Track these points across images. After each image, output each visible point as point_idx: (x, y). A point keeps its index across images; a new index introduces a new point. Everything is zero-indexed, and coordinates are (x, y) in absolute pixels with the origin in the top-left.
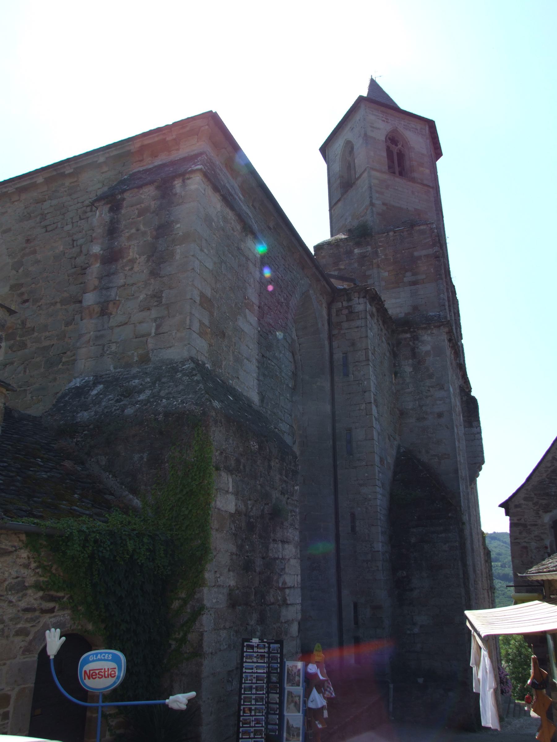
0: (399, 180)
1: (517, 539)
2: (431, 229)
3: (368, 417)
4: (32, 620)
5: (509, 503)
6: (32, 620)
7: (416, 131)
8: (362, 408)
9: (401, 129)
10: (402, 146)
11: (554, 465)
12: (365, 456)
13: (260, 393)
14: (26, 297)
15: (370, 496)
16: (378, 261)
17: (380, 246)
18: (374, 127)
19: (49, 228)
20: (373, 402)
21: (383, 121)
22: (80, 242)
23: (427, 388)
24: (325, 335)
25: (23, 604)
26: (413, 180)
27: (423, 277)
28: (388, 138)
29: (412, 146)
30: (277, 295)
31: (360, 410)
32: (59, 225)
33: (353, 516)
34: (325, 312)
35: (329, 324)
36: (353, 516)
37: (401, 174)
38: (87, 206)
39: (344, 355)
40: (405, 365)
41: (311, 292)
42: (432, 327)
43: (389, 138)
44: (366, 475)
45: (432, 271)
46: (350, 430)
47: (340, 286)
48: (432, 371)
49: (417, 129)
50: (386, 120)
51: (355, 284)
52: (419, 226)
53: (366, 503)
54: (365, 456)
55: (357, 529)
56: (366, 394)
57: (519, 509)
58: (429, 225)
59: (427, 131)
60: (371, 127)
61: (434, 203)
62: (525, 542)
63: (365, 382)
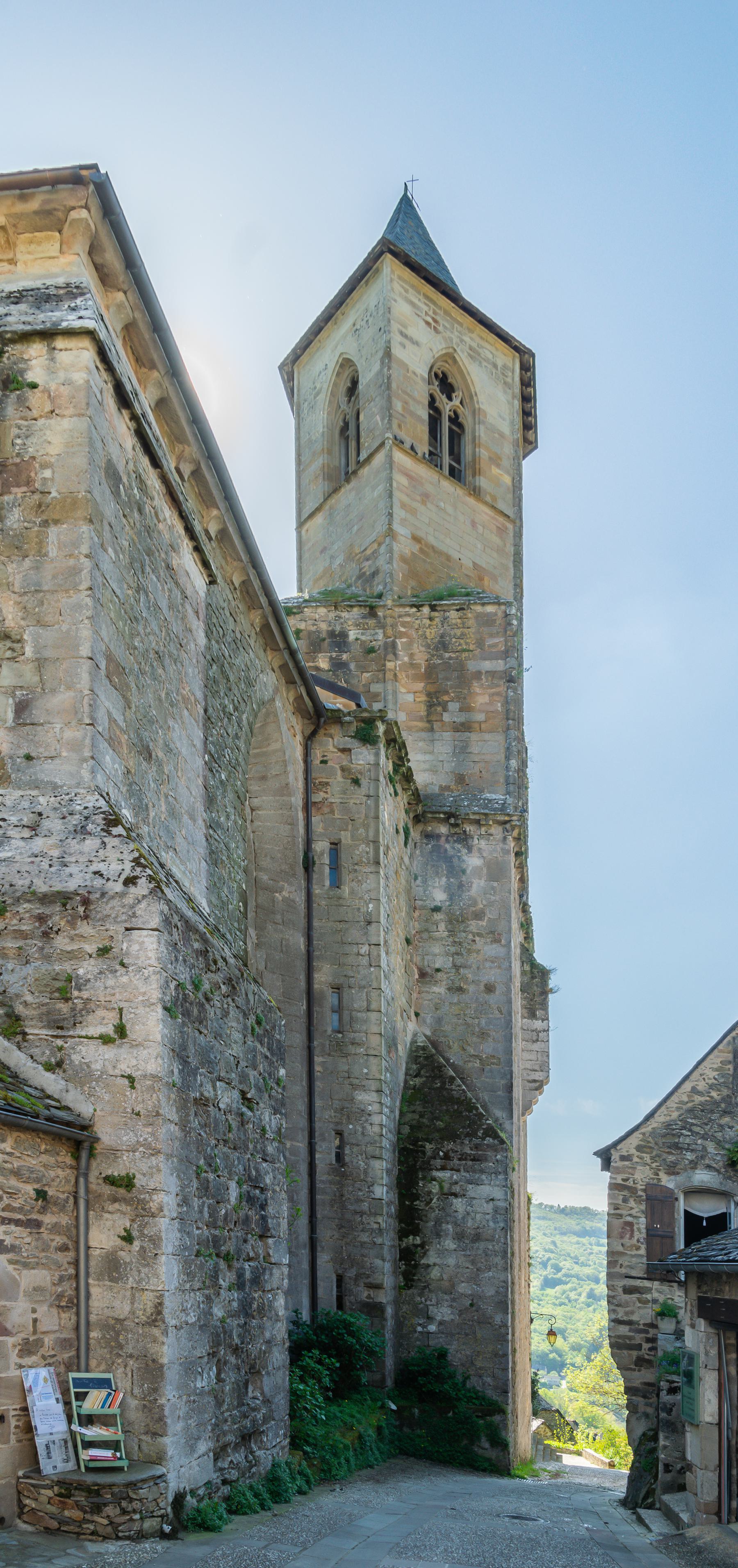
0: (448, 485)
1: (618, 1209)
2: (506, 615)
3: (372, 969)
5: (613, 1151)
7: (494, 371)
8: (362, 951)
9: (463, 357)
11: (693, 1101)
12: (364, 1039)
15: (370, 1108)
16: (396, 667)
17: (402, 635)
18: (406, 336)
20: (382, 944)
21: (428, 323)
23: (470, 937)
24: (298, 800)
26: (476, 492)
27: (481, 717)
28: (433, 374)
29: (481, 406)
30: (222, 694)
31: (358, 954)
34: (298, 753)
35: (306, 779)
37: (455, 474)
39: (333, 846)
40: (434, 887)
41: (278, 704)
42: (491, 823)
43: (436, 375)
44: (365, 1071)
45: (500, 709)
46: (338, 989)
48: (482, 906)
50: (433, 324)
51: (358, 705)
52: (483, 604)
53: (363, 1118)
54: (364, 1039)
55: (347, 1159)
56: (372, 928)
57: (627, 1163)
58: (503, 607)
60: (401, 333)
61: (512, 558)
62: (630, 1215)
63: (371, 906)
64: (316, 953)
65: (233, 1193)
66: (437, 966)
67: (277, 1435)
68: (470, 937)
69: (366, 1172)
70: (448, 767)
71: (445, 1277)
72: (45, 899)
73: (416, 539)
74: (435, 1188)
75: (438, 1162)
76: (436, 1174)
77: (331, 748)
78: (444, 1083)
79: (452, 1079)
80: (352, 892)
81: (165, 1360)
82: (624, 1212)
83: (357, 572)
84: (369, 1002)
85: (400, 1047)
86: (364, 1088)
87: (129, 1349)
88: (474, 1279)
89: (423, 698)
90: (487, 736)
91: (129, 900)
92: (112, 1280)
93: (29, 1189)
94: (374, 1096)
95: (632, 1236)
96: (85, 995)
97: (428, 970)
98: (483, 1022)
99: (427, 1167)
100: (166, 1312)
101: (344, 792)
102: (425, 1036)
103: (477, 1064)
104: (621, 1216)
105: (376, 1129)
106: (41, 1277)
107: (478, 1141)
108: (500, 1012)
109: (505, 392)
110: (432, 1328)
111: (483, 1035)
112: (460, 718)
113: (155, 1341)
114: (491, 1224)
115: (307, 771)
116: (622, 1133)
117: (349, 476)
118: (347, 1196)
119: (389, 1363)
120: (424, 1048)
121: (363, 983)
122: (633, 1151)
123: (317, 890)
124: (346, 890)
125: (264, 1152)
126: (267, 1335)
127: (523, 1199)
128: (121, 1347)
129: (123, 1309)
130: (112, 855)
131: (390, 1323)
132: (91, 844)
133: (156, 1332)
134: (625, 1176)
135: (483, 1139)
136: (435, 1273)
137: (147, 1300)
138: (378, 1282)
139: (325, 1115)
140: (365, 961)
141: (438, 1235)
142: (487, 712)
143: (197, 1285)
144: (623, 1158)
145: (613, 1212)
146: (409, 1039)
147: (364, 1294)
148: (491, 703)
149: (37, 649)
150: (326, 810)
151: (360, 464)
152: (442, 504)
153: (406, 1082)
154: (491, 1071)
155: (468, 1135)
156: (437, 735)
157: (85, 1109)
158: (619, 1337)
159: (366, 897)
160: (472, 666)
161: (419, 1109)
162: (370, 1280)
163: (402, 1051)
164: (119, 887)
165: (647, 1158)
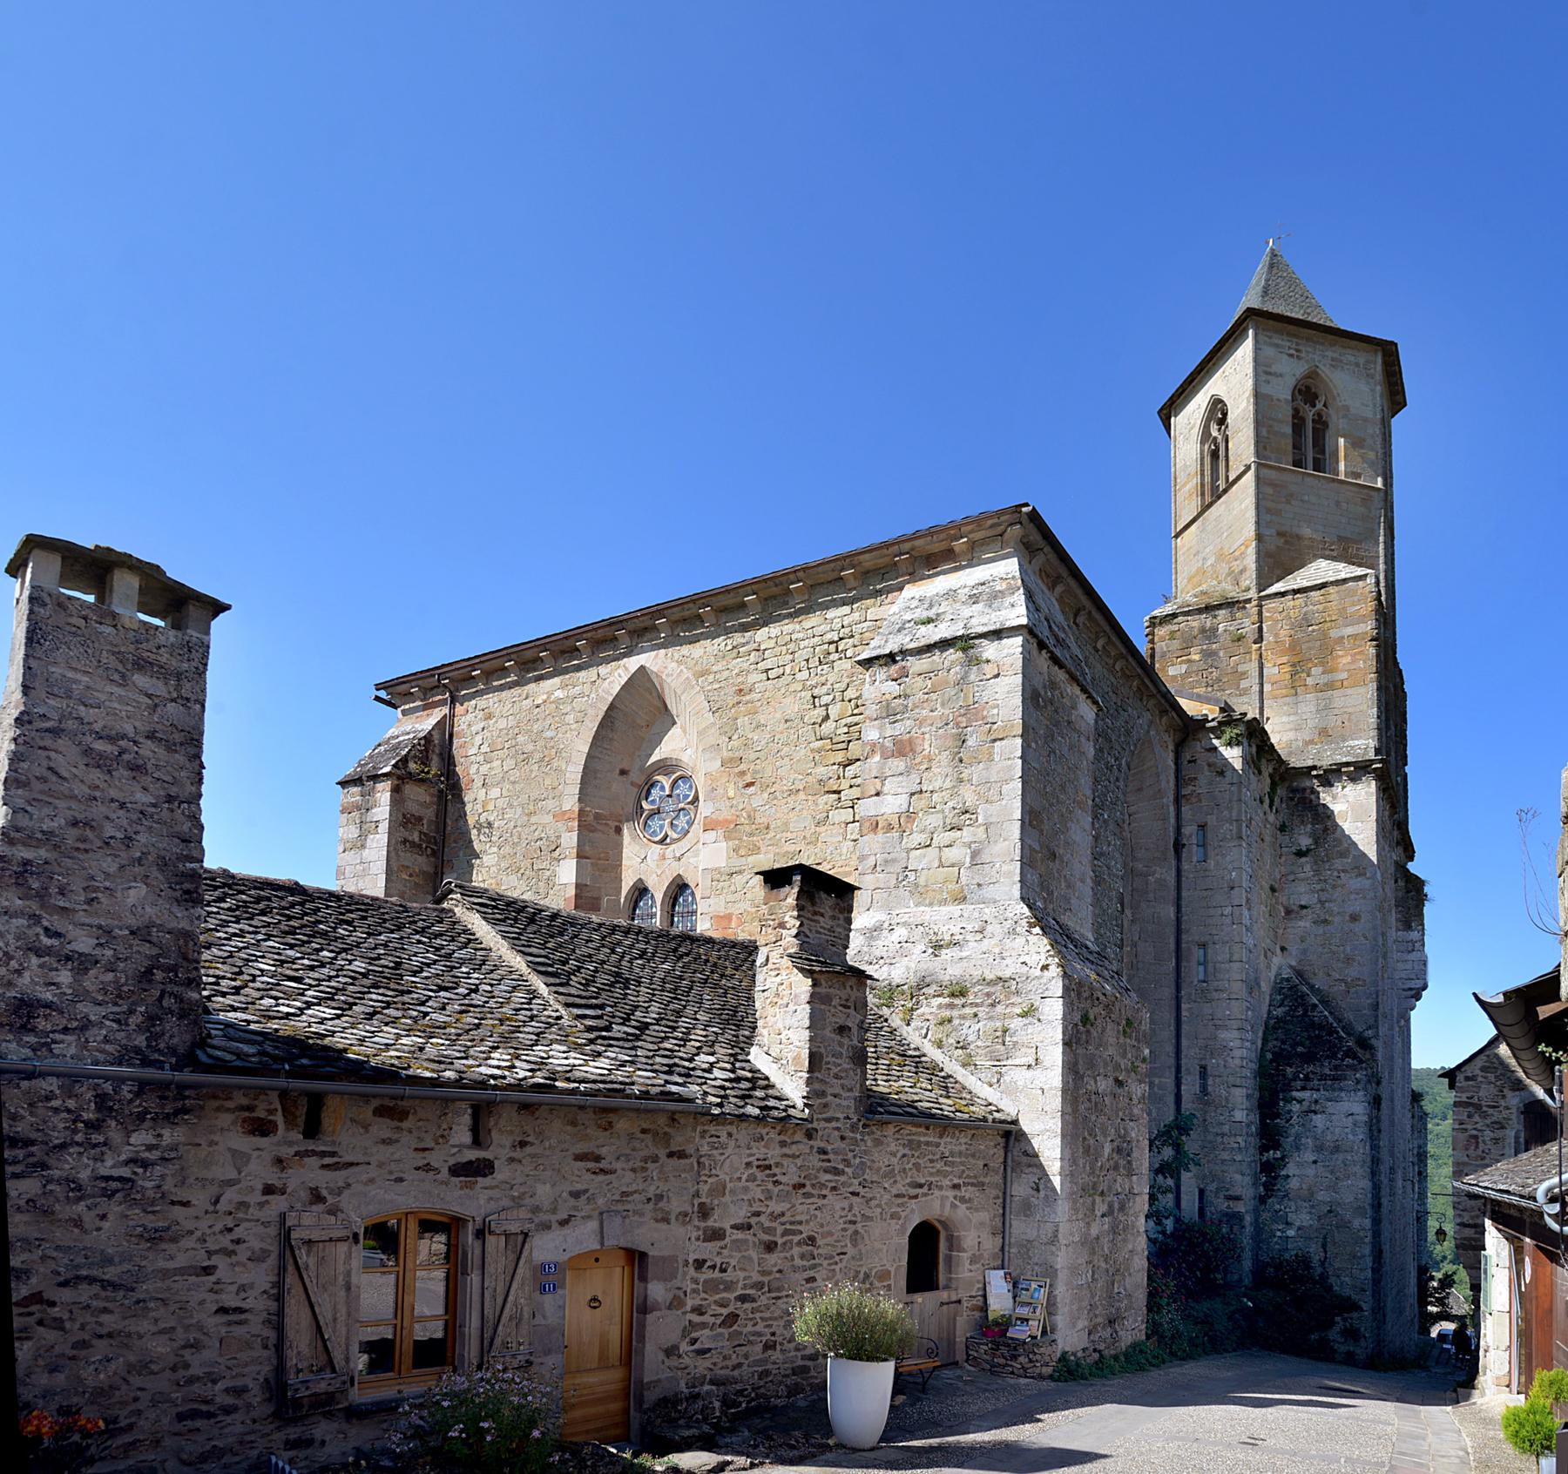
4: (902, 1204)
6: (902, 1204)
8: (1226, 913)
10: (1325, 405)
13: (1097, 932)
14: (749, 779)
18: (1270, 374)
19: (772, 674)
21: (1291, 356)
22: (826, 699)
23: (1336, 874)
25: (894, 1191)
27: (1344, 675)
32: (788, 671)
33: (1204, 1069)
35: (1177, 777)
36: (1204, 1069)
37: (1318, 467)
38: (830, 643)
43: (1300, 391)
47: (1199, 698)
49: (1357, 365)
55: (1210, 1089)
59: (1379, 367)
64: (1185, 918)
65: (1107, 1149)
66: (1303, 903)
67: (1136, 1321)
68: (1336, 874)
69: (1227, 1099)
70: (1311, 724)
71: (1304, 1186)
72: (991, 983)
73: (1280, 534)
74: (1295, 1107)
75: (1299, 1084)
76: (1295, 1094)
77: (1199, 749)
78: (1306, 1011)
79: (1315, 1006)
80: (1217, 864)
81: (1059, 1267)
82: (1469, 1127)
83: (1227, 571)
84: (1231, 954)
85: (1263, 984)
86: (1226, 1027)
87: (1036, 1260)
88: (1333, 1188)
89: (1287, 669)
90: (1349, 691)
91: (1044, 981)
92: (1026, 1216)
93: (981, 1163)
94: (1235, 1034)
95: (1477, 1147)
96: (1015, 1039)
97: (1295, 908)
98: (1348, 948)
99: (1288, 1088)
100: (1060, 1236)
101: (1210, 784)
102: (1291, 967)
103: (1343, 987)
104: (1466, 1130)
105: (1238, 1062)
106: (984, 1216)
107: (1338, 1062)
108: (1366, 938)
109: (1368, 383)
110: (1291, 1233)
111: (1348, 960)
112: (1324, 679)
113: (1053, 1253)
114: (1350, 1136)
115: (1178, 771)
116: (1466, 1056)
117: (1217, 495)
118: (1209, 1120)
119: (1247, 1264)
120: (1288, 980)
121: (1226, 939)
122: (1477, 1072)
123: (1185, 866)
124: (1211, 863)
125: (1131, 1114)
126: (1130, 1247)
127: (1402, 1102)
128: (1030, 1258)
129: (1032, 1234)
130: (1033, 949)
131: (1249, 1229)
132: (1020, 941)
133: (1054, 1248)
134: (1469, 1095)
135: (1343, 1060)
136: (1294, 1184)
137: (1049, 1228)
138: (1238, 1194)
139: (1190, 1053)
140: (1228, 920)
141: (1298, 1149)
142: (1348, 671)
143: (1080, 1216)
144: (1467, 1079)
145: (1457, 1127)
146: (1272, 975)
147: (1223, 1205)
148: (1353, 662)
149: (986, 817)
150: (1194, 800)
151: (1230, 485)
152: (1306, 498)
153: (1269, 1012)
154: (1356, 992)
155: (1328, 1057)
156: (1300, 698)
157: (1009, 1108)
158: (1465, 1239)
159: (1230, 867)
160: (1334, 634)
161: (1282, 1036)
162: (1230, 1193)
163: (1266, 987)
164: (1038, 972)
165: (1491, 1077)
